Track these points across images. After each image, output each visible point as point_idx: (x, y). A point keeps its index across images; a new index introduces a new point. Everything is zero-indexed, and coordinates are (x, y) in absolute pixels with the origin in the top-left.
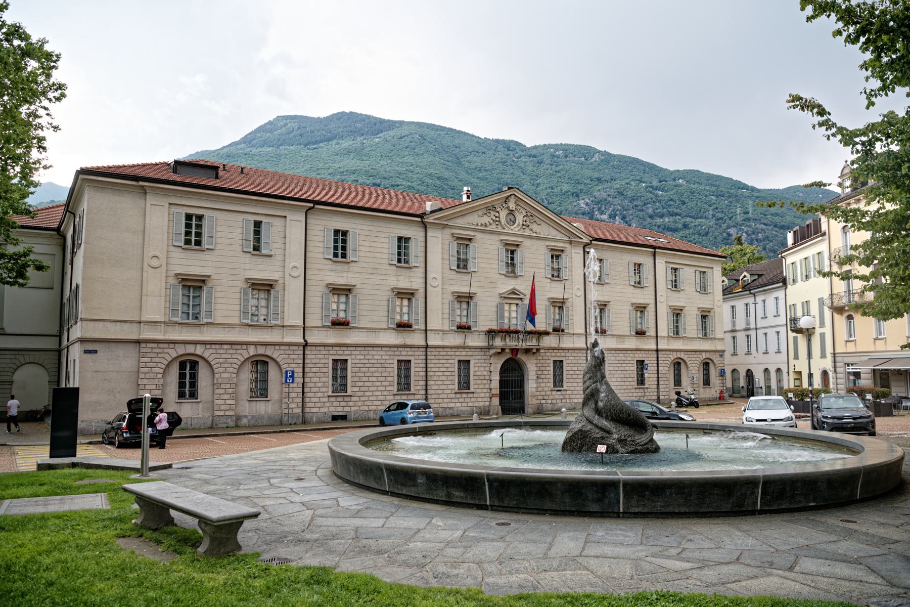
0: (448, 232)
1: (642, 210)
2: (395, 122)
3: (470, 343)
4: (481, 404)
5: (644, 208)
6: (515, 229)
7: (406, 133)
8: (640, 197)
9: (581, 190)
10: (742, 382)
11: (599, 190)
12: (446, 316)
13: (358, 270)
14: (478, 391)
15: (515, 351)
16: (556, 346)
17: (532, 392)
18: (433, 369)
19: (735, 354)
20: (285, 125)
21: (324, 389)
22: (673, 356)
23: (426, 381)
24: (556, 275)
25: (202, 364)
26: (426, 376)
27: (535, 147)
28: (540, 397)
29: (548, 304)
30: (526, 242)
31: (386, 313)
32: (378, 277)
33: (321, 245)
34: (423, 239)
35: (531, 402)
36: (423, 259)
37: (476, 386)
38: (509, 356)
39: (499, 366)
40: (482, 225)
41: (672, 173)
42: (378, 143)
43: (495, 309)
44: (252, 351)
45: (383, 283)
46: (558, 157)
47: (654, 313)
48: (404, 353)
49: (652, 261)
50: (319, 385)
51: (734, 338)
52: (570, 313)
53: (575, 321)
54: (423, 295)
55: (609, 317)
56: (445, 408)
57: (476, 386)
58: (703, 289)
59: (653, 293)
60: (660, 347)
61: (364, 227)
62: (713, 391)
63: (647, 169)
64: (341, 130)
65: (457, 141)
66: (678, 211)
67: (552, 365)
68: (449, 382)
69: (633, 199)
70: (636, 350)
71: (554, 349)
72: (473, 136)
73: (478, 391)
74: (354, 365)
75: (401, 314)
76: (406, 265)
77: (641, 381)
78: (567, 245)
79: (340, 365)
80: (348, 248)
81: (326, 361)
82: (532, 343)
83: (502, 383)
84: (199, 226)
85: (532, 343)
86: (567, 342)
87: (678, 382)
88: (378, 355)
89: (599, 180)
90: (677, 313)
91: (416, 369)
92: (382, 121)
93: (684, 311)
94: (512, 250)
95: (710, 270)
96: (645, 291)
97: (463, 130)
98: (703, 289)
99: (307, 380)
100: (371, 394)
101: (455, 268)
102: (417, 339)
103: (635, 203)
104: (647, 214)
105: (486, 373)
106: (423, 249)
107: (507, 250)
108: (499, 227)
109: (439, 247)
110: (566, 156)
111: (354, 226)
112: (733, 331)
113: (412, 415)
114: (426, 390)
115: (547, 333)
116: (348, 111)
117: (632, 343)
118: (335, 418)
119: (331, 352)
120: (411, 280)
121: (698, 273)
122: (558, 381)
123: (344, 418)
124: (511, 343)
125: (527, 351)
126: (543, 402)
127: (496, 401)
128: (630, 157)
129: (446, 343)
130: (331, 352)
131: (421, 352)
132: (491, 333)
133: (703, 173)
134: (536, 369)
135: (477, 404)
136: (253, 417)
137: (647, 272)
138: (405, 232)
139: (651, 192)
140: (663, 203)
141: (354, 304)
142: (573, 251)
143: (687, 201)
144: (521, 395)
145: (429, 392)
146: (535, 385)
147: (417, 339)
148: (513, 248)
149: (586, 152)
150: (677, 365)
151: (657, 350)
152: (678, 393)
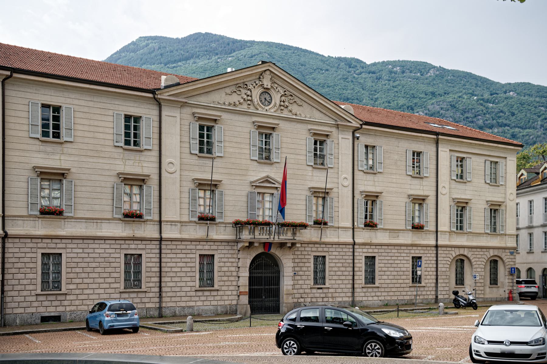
0: (188, 111)
1: (472, 122)
2: (247, 42)
3: (214, 235)
4: (227, 303)
5: (475, 120)
6: (271, 110)
7: (257, 52)
8: (472, 109)
9: (416, 104)
11: (433, 104)
12: (186, 206)
13: (74, 152)
14: (223, 288)
15: (267, 245)
16: (318, 240)
17: (287, 290)
18: (169, 265)
19: (530, 252)
20: (147, 45)
21: (31, 287)
22: (455, 253)
23: (160, 277)
27: (374, 64)
28: (297, 296)
29: (309, 194)
30: (283, 125)
31: (110, 202)
32: (101, 160)
33: (25, 121)
34: (157, 119)
36: (156, 142)
37: (222, 283)
38: (261, 250)
39: (249, 262)
40: (230, 104)
41: (503, 86)
42: (231, 62)
43: (245, 199)
45: (107, 167)
46: (395, 73)
47: (434, 206)
48: (133, 246)
50: (25, 282)
51: (530, 234)
52: (335, 204)
53: (342, 212)
54: (156, 182)
55: (381, 209)
56: (184, 307)
57: (222, 283)
58: (494, 180)
59: (435, 184)
60: (440, 243)
61: (82, 103)
62: (501, 291)
63: (480, 83)
64: (197, 50)
65: (302, 59)
66: (507, 122)
67: (312, 260)
68: (189, 279)
69: (464, 112)
70: (412, 245)
71: (315, 243)
72: (318, 54)
73: (223, 288)
74: (330, 261)
75: (131, 202)
77: (416, 279)
78: (334, 130)
79: (371, 260)
82: (287, 236)
83: (252, 280)
85: (287, 236)
86: (330, 236)
87: (460, 281)
88: (100, 248)
89: (433, 94)
90: (462, 207)
91: (149, 264)
92: (235, 41)
93: (469, 205)
94: (266, 133)
95: (503, 160)
96: (425, 182)
97: (308, 49)
98: (494, 180)
100: (91, 292)
101: (197, 152)
102: (149, 231)
103: (466, 115)
104: (477, 125)
105: (233, 269)
106: (157, 130)
107: (261, 134)
108: (251, 107)
110: (403, 72)
111: (68, 101)
112: (530, 227)
113: (109, 318)
114: (160, 287)
115: (304, 226)
116: (203, 32)
117: (408, 238)
118: (45, 319)
119: (40, 245)
120: (142, 165)
121: (488, 163)
122: (319, 277)
123: (57, 319)
124: (261, 236)
125: (282, 245)
126: (302, 300)
127: (245, 299)
128: (463, 72)
129: (185, 236)
130: (40, 245)
131: (154, 246)
132: (238, 225)
133: (534, 86)
134: (292, 265)
135: (222, 303)
137: (428, 161)
138: (134, 110)
139: (482, 105)
140: (493, 115)
141: (69, 190)
142: (340, 136)
143: (516, 112)
144: (276, 293)
145: (164, 289)
146: (292, 283)
147: (149, 231)
149: (422, 68)
150: (460, 263)
151: (437, 246)
152: (456, 293)
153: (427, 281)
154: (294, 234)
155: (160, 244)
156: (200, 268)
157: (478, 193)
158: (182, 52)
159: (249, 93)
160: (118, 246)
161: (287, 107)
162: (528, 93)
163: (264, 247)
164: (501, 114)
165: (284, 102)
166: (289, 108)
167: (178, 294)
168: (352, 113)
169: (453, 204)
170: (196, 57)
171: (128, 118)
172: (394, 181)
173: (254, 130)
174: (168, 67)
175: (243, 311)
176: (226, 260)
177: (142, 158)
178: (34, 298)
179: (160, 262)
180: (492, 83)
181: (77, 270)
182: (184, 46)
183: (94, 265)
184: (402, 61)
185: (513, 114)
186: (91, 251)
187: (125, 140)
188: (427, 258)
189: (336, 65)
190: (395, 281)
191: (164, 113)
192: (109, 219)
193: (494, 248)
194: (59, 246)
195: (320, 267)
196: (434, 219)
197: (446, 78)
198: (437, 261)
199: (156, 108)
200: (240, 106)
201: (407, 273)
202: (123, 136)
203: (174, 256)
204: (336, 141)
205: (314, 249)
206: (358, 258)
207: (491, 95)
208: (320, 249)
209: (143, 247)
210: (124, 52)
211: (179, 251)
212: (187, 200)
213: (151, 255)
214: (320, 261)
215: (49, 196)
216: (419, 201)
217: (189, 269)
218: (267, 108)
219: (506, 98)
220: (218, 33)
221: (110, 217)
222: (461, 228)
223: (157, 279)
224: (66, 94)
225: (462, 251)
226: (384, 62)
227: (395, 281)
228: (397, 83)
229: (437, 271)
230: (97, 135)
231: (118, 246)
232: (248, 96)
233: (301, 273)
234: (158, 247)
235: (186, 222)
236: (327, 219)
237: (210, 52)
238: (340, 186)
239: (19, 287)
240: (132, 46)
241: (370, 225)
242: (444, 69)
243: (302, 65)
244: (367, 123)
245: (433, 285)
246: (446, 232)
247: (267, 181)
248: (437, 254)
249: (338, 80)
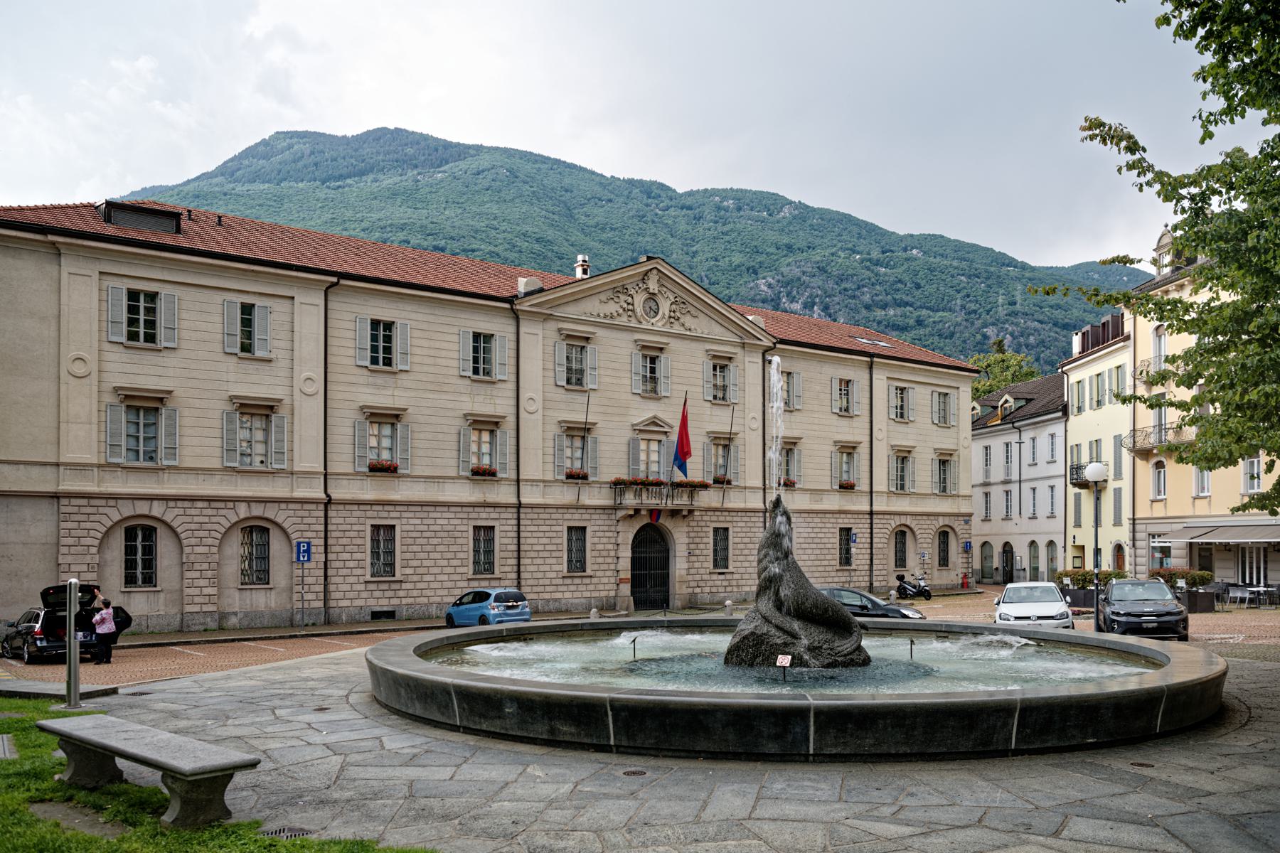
0: (552, 326)
1: (854, 297)
2: (469, 147)
3: (586, 500)
4: (603, 594)
5: (858, 293)
6: (658, 323)
7: (487, 165)
10: (997, 562)
11: (789, 265)
12: (550, 459)
14: (599, 574)
15: (655, 513)
16: (718, 505)
17: (681, 576)
18: (529, 541)
19: (987, 519)
20: (290, 147)
21: (359, 572)
22: (894, 522)
24: (720, 396)
25: (161, 532)
27: (690, 194)
28: (693, 584)
29: (707, 440)
30: (674, 345)
31: (455, 454)
32: (444, 397)
34: (513, 337)
35: (679, 590)
36: (513, 369)
37: (596, 567)
38: (646, 521)
39: (631, 536)
42: (442, 181)
43: (625, 448)
45: (451, 405)
46: (726, 209)
48: (483, 515)
49: (868, 376)
50: (352, 564)
51: (987, 494)
52: (741, 455)
55: (799, 461)
56: (548, 600)
57: (596, 567)
58: (944, 420)
59: (868, 426)
60: (875, 508)
61: (420, 317)
62: (953, 574)
64: (381, 158)
65: (567, 181)
66: (909, 299)
69: (840, 279)
70: (840, 512)
71: (715, 510)
72: (593, 173)
73: (599, 574)
75: (479, 455)
76: (487, 378)
77: (846, 559)
78: (738, 350)
80: (394, 350)
81: (362, 527)
82: (682, 501)
83: (635, 562)
85: (682, 501)
86: (735, 500)
87: (901, 561)
88: (443, 519)
89: (789, 247)
90: (903, 457)
91: (503, 540)
92: (447, 145)
94: (652, 356)
98: (944, 420)
99: (331, 557)
101: (564, 383)
103: (844, 285)
105: (610, 547)
106: (513, 353)
107: (645, 357)
108: (633, 319)
110: (739, 209)
111: (404, 314)
112: (986, 484)
114: (519, 572)
115: (704, 486)
117: (834, 502)
118: (376, 616)
119: (369, 514)
121: (936, 395)
123: (390, 615)
124: (650, 501)
125: (674, 513)
126: (698, 590)
127: (626, 589)
128: (837, 213)
129: (550, 501)
130: (369, 514)
131: (510, 515)
134: (687, 540)
136: (246, 614)
138: (484, 324)
139: (868, 269)
142: (747, 359)
143: (923, 283)
145: (523, 575)
147: (505, 494)
148: (654, 353)
149: (771, 203)
150: (901, 536)
151: (871, 513)
152: (901, 578)
154: (691, 497)
155: (518, 513)
156: (372, 548)
157: (924, 438)
158: (353, 161)
159: (630, 300)
160: (465, 516)
161: (678, 319)
162: (941, 252)
163: (651, 517)
164: (900, 285)
167: (541, 582)
168: (763, 326)
169: (891, 453)
170: (379, 171)
171: (375, 324)
172: (816, 421)
173: (635, 351)
174: (328, 187)
175: (625, 605)
176: (601, 534)
177: (495, 393)
178: (362, 587)
179: (519, 537)
180: (884, 233)
181: (415, 548)
182: (356, 150)
183: (435, 541)
184: (737, 190)
185: (918, 286)
186: (432, 522)
189: (626, 193)
190: (817, 563)
191: (522, 330)
192: (453, 478)
193: (944, 515)
195: (720, 545)
196: (868, 475)
197: (809, 222)
198: (871, 533)
199: (513, 322)
200: (619, 319)
201: (833, 551)
203: (535, 528)
204: (741, 367)
205: (714, 518)
206: (334, 521)
207: (883, 252)
208: (722, 519)
209: (496, 516)
210: (247, 157)
211: (541, 522)
212: (551, 451)
214: (722, 535)
215: (379, 444)
216: (848, 449)
217: (554, 548)
218: (653, 321)
219: (907, 259)
220: (418, 130)
221: (454, 474)
222: (902, 487)
223: (514, 562)
224: (401, 306)
225: (904, 520)
226: (706, 190)
227: (817, 563)
228: (729, 227)
229: (871, 548)
230: (439, 361)
231: (465, 516)
233: (697, 552)
234: (515, 516)
236: (728, 477)
237: (405, 162)
238: (747, 429)
239: (345, 572)
240: (262, 148)
242: (807, 207)
243: (567, 191)
245: (867, 567)
246: (92, 465)
248: (871, 524)
249: (629, 218)
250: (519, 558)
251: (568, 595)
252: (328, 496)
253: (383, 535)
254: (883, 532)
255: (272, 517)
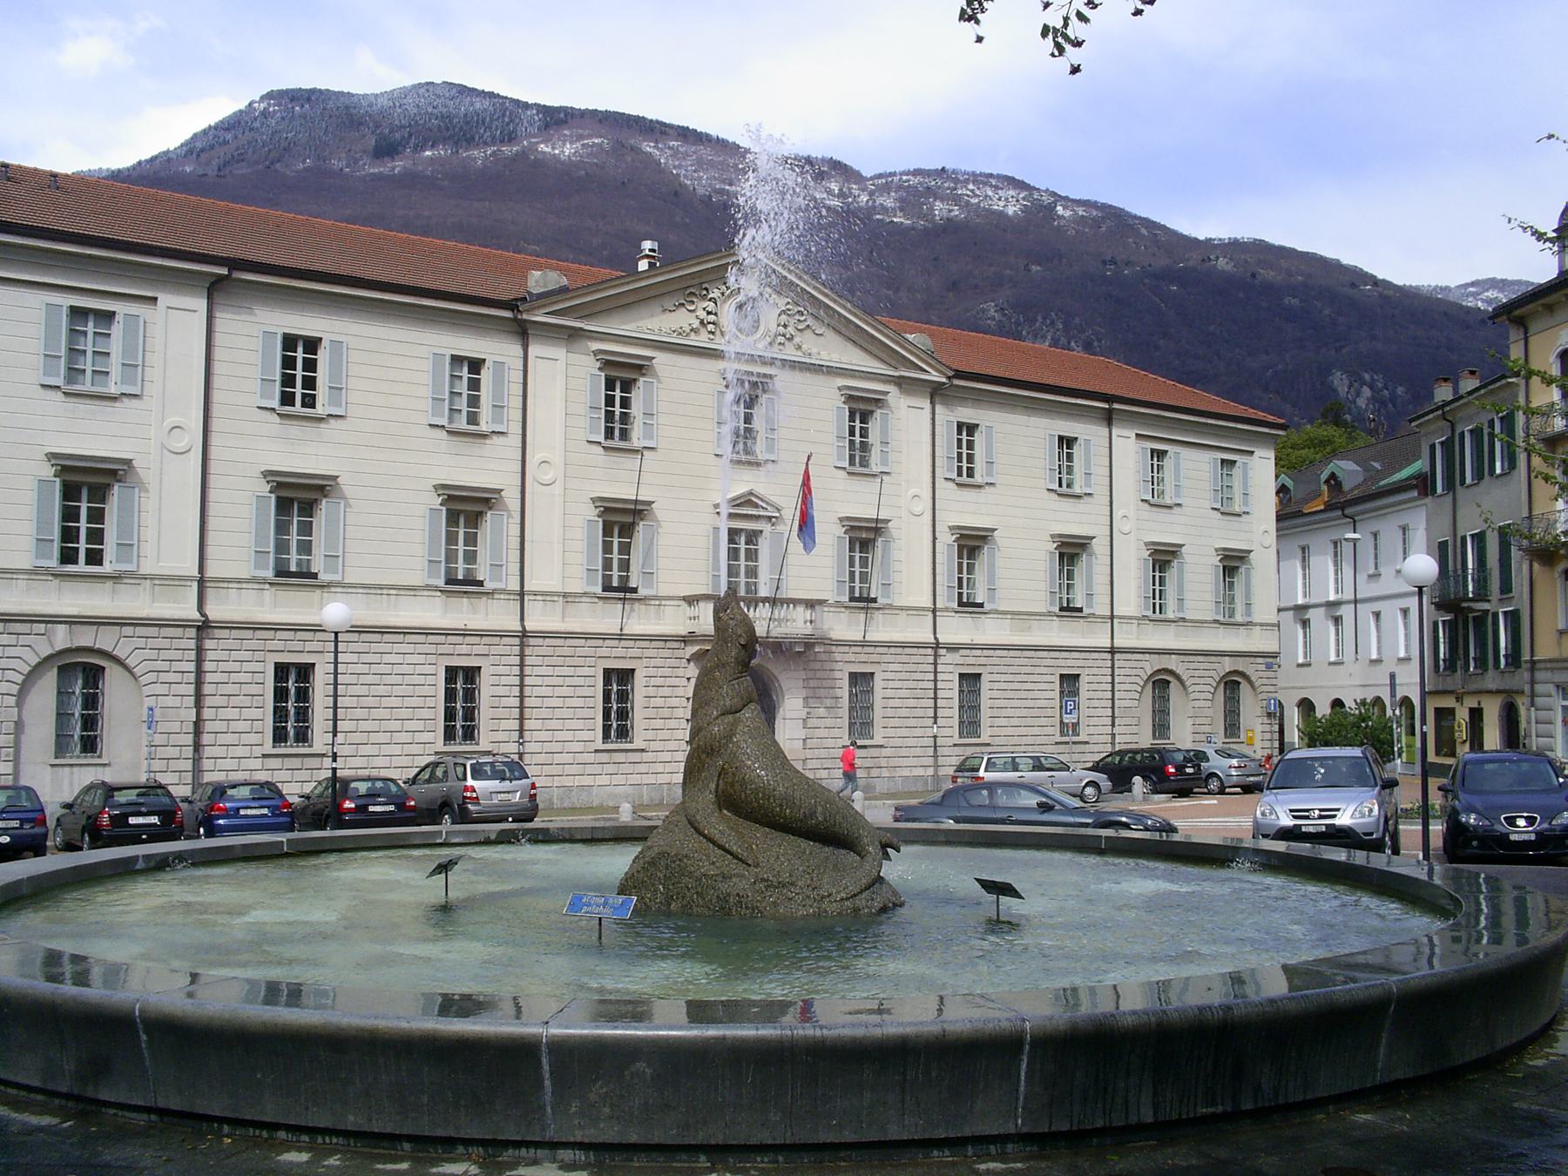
18: (352, 690)
21: (253, 738)
22: (1151, 665)
24: (858, 454)
26: (522, 707)
30: (661, 360)
44: (61, 638)
48: (464, 649)
60: (529, 626)
76: (622, 444)
79: (970, 681)
80: (319, 383)
81: (258, 667)
84: (310, 365)
88: (395, 653)
91: (493, 691)
99: (207, 713)
109: (561, 381)
119: (271, 645)
130: (271, 645)
135: (651, 779)
146: (802, 734)
147: (500, 615)
153: (1092, 730)
165: (785, 326)
166: (797, 340)
171: (290, 342)
187: (283, 393)
188: (1091, 679)
194: (309, 646)
202: (278, 384)
213: (501, 670)
231: (432, 649)
232: (709, 313)
235: (576, 595)
241: (968, 605)
244: (959, 374)
246: (1131, 618)
247: (749, 503)
250: (522, 719)
251: (604, 780)
252: (523, 626)
253: (293, 680)
254: (1134, 674)
255: (90, 644)
